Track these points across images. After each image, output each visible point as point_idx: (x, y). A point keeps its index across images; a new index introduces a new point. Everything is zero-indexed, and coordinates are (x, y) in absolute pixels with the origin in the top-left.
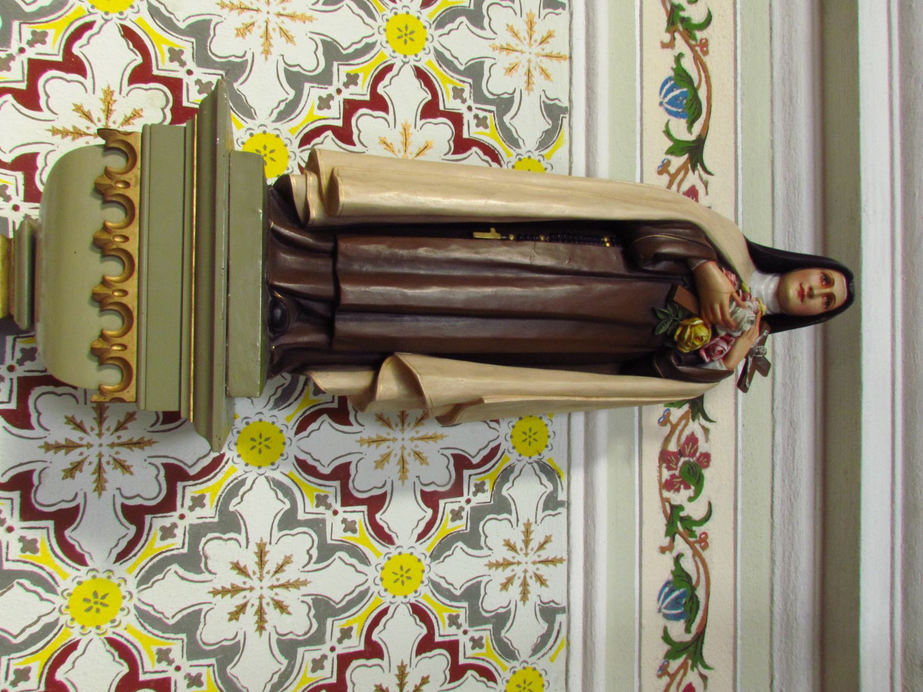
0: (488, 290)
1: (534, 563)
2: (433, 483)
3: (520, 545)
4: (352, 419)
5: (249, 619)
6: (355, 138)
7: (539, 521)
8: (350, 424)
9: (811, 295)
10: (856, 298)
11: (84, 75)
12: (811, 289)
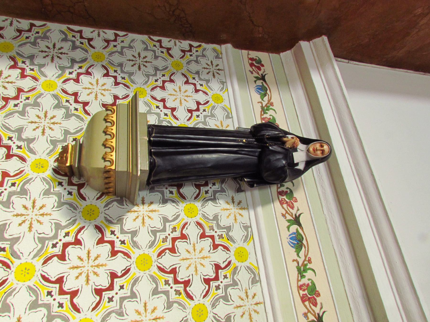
0: (172, 140)
1: (245, 305)
2: (155, 227)
3: (253, 313)
4: (125, 204)
5: (38, 204)
6: (166, 89)
7: (250, 288)
8: (124, 205)
9: (317, 150)
10: (332, 151)
11: (174, 83)
12: (316, 148)
